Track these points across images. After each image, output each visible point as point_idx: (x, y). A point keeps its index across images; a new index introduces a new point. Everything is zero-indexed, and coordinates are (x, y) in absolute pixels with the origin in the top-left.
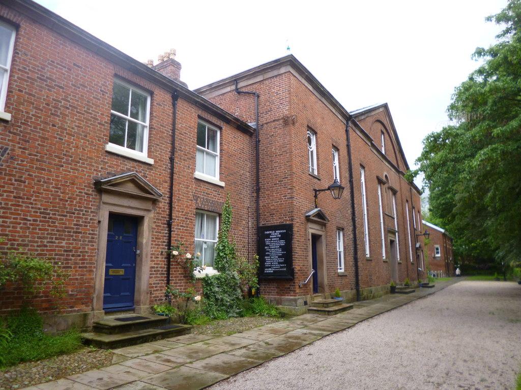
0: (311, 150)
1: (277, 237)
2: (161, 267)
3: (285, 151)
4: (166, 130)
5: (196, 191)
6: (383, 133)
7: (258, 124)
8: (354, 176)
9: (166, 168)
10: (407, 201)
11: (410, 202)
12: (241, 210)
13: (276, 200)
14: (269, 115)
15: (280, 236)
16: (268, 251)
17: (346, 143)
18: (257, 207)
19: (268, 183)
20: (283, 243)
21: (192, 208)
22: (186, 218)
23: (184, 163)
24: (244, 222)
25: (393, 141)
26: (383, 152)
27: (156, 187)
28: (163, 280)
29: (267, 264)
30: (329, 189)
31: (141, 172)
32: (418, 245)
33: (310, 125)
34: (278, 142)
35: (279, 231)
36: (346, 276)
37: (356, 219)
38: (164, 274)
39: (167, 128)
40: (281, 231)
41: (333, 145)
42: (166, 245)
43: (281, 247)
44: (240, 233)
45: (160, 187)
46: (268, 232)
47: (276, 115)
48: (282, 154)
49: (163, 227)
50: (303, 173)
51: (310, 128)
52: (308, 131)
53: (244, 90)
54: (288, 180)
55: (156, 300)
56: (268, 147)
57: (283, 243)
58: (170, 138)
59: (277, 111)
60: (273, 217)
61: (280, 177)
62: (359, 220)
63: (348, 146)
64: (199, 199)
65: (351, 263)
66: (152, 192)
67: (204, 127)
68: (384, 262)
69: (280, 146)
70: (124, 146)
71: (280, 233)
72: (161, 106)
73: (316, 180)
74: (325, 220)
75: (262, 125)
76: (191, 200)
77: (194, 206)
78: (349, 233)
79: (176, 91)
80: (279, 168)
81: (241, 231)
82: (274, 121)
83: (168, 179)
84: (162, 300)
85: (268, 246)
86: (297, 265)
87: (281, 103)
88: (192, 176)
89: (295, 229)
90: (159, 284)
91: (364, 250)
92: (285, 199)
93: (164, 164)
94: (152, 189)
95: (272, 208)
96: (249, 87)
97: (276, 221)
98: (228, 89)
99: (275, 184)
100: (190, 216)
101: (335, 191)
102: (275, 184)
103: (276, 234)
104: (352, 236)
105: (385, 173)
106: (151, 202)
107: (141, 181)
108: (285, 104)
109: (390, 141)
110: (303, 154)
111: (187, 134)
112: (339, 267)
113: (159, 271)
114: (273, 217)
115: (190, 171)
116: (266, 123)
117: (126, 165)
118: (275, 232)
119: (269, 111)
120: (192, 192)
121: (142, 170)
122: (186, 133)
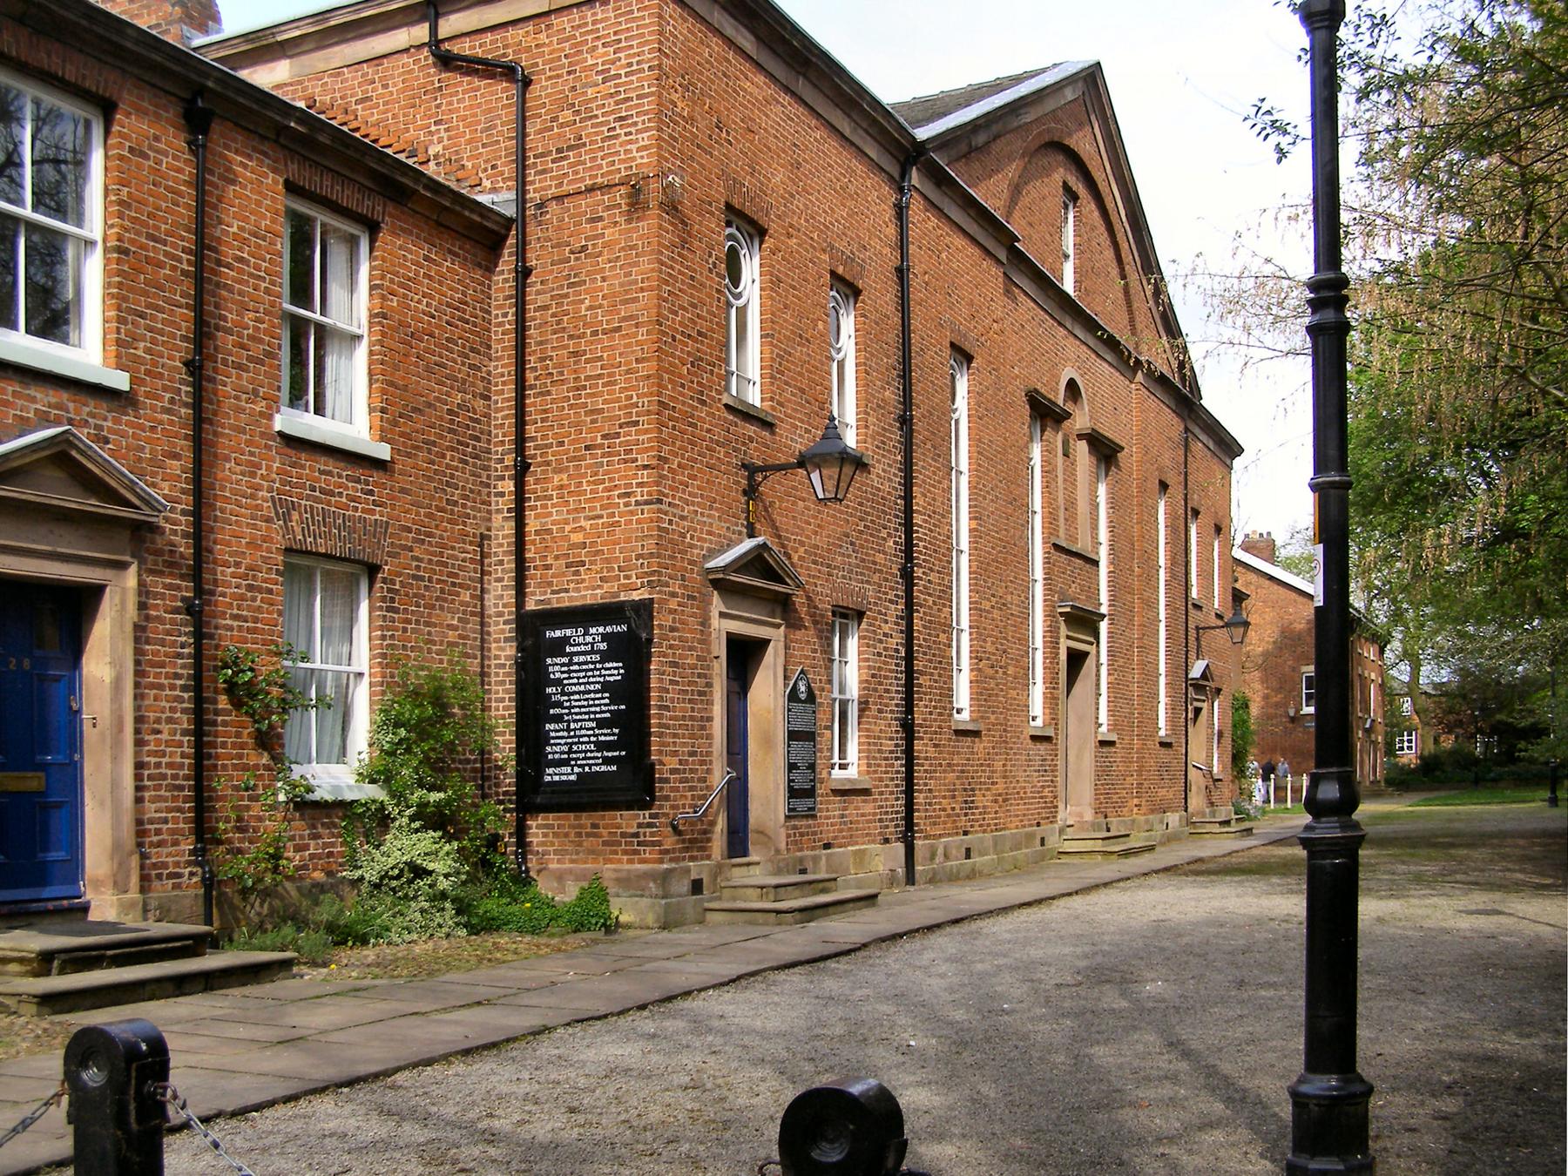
0: (741, 302)
1: (592, 652)
2: (170, 765)
3: (631, 317)
4: (166, 254)
5: (283, 483)
6: (1074, 197)
7: (522, 200)
8: (917, 398)
9: (172, 401)
10: (1164, 486)
11: (1176, 490)
12: (453, 548)
13: (591, 509)
14: (571, 165)
15: (603, 646)
16: (559, 705)
17: (892, 258)
18: (524, 286)
19: (561, 444)
20: (614, 672)
21: (269, 550)
22: (250, 588)
23: (239, 377)
24: (466, 596)
25: (1117, 226)
26: (1068, 286)
27: (141, 475)
28: (180, 810)
29: (554, 751)
30: (801, 464)
31: (86, 423)
32: (1196, 671)
33: (736, 203)
34: (604, 279)
35: (601, 630)
36: (866, 792)
37: (918, 572)
38: (181, 788)
39: (174, 246)
40: (609, 629)
41: (833, 273)
42: (184, 688)
43: (606, 686)
44: (452, 636)
45: (154, 474)
46: (558, 633)
47: (600, 167)
48: (619, 329)
49: (173, 622)
50: (703, 403)
51: (733, 214)
52: (729, 224)
53: (464, 48)
54: (638, 433)
55: (159, 876)
56: (566, 296)
57: (614, 672)
58: (188, 286)
59: (601, 149)
60: (577, 573)
61: (610, 419)
62: (933, 576)
63: (902, 273)
64: (295, 515)
65: (889, 745)
66: (129, 496)
67: (310, 221)
68: (1162, 744)
69: (614, 295)
70: (13, 326)
71: (605, 637)
72: (146, 157)
73: (751, 430)
74: (782, 581)
75: (540, 206)
76: (268, 520)
77: (280, 541)
78: (886, 628)
79: (201, 91)
80: (604, 385)
81: (455, 628)
82: (591, 190)
83: (184, 446)
84: (179, 875)
85: (558, 682)
86: (665, 754)
87: (622, 119)
88: (270, 427)
89: (661, 620)
90: (166, 821)
91: (948, 693)
92: (627, 505)
93: (165, 389)
94: (132, 487)
95: (577, 538)
96: (489, 37)
97: (588, 594)
98: (400, 38)
99: (587, 448)
100: (265, 581)
101: (825, 472)
102: (587, 448)
103: (589, 639)
104: (897, 640)
105: (1067, 373)
106: (127, 534)
107: (89, 458)
108: (635, 124)
109: (1102, 229)
110: (702, 325)
111: (247, 263)
112: (836, 760)
113: (164, 777)
114: (577, 573)
115: (260, 406)
116: (559, 198)
117: (33, 400)
118: (586, 633)
119: (570, 148)
120: (270, 490)
121: (89, 414)
122: (241, 260)
